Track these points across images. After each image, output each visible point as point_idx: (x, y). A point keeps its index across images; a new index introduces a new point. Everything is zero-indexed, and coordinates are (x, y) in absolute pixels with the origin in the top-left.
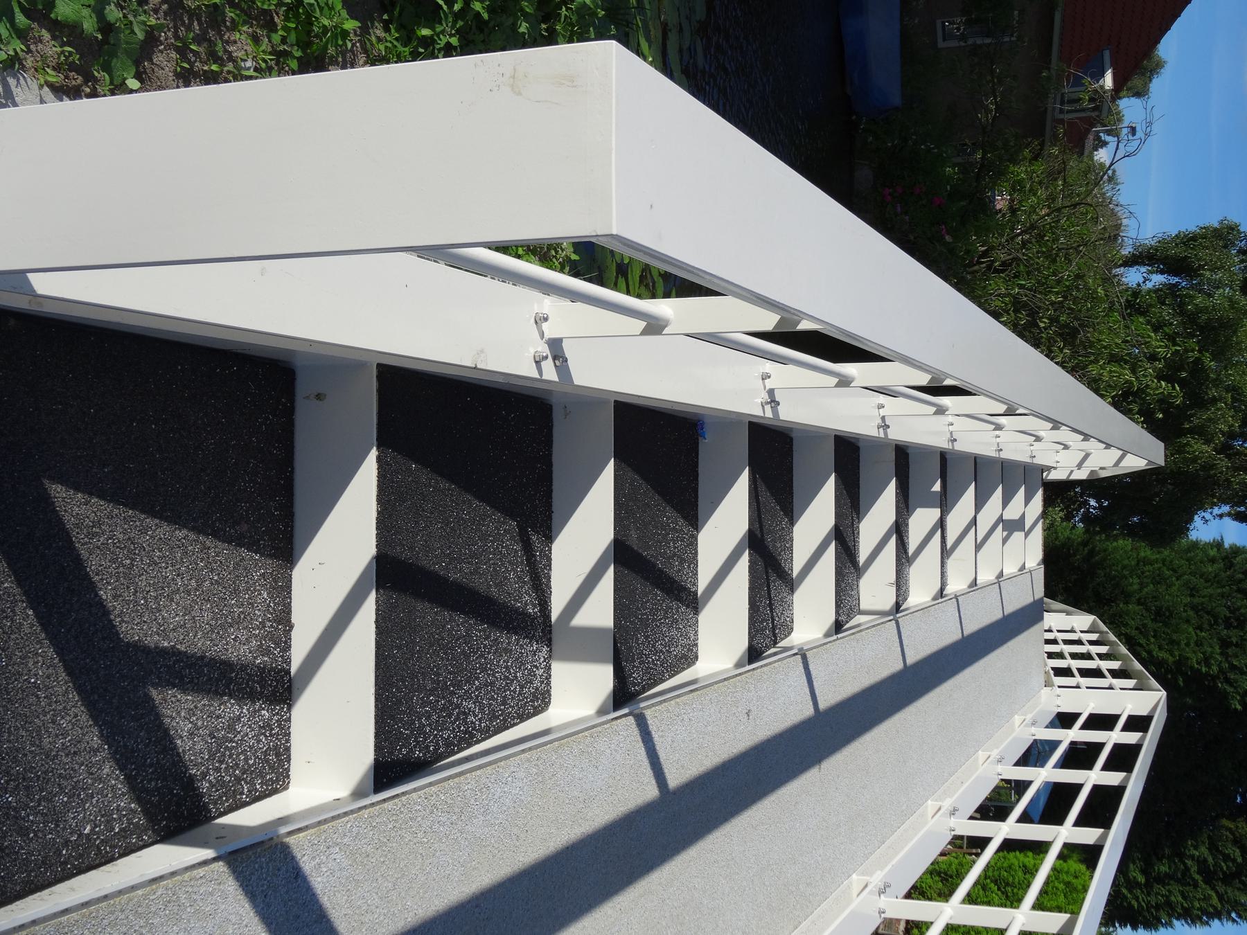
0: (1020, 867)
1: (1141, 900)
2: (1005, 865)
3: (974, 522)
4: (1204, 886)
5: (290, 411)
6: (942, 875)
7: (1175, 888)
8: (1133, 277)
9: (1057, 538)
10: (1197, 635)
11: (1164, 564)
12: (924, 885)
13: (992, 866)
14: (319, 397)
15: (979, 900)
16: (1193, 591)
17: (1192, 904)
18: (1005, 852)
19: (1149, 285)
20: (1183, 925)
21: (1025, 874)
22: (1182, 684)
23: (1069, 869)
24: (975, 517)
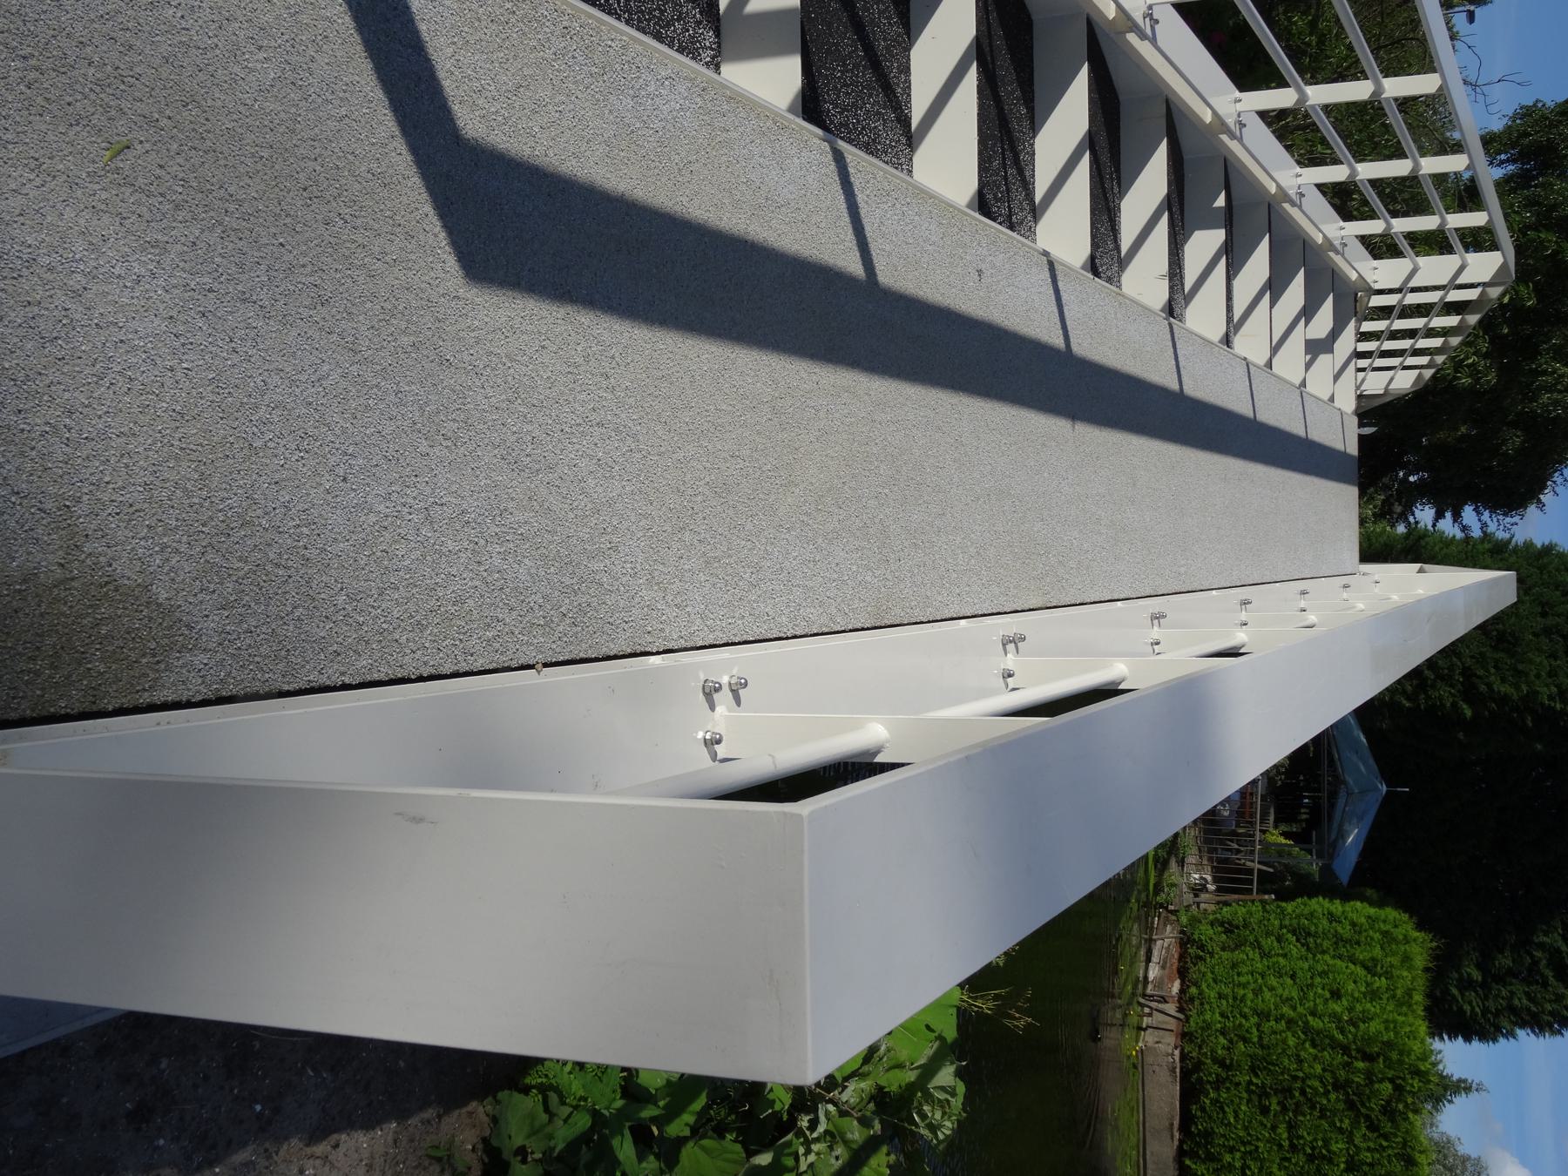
0: (1324, 915)
1: (1474, 1004)
2: (1306, 912)
4: (1555, 983)
6: (1226, 925)
7: (1519, 988)
10: (1550, 665)
12: (1203, 938)
13: (1289, 914)
15: (1273, 953)
17: (1542, 1007)
18: (1306, 898)
20: (1528, 1034)
21: (1331, 923)
22: (1530, 724)
23: (1387, 917)
24: (1271, 359)
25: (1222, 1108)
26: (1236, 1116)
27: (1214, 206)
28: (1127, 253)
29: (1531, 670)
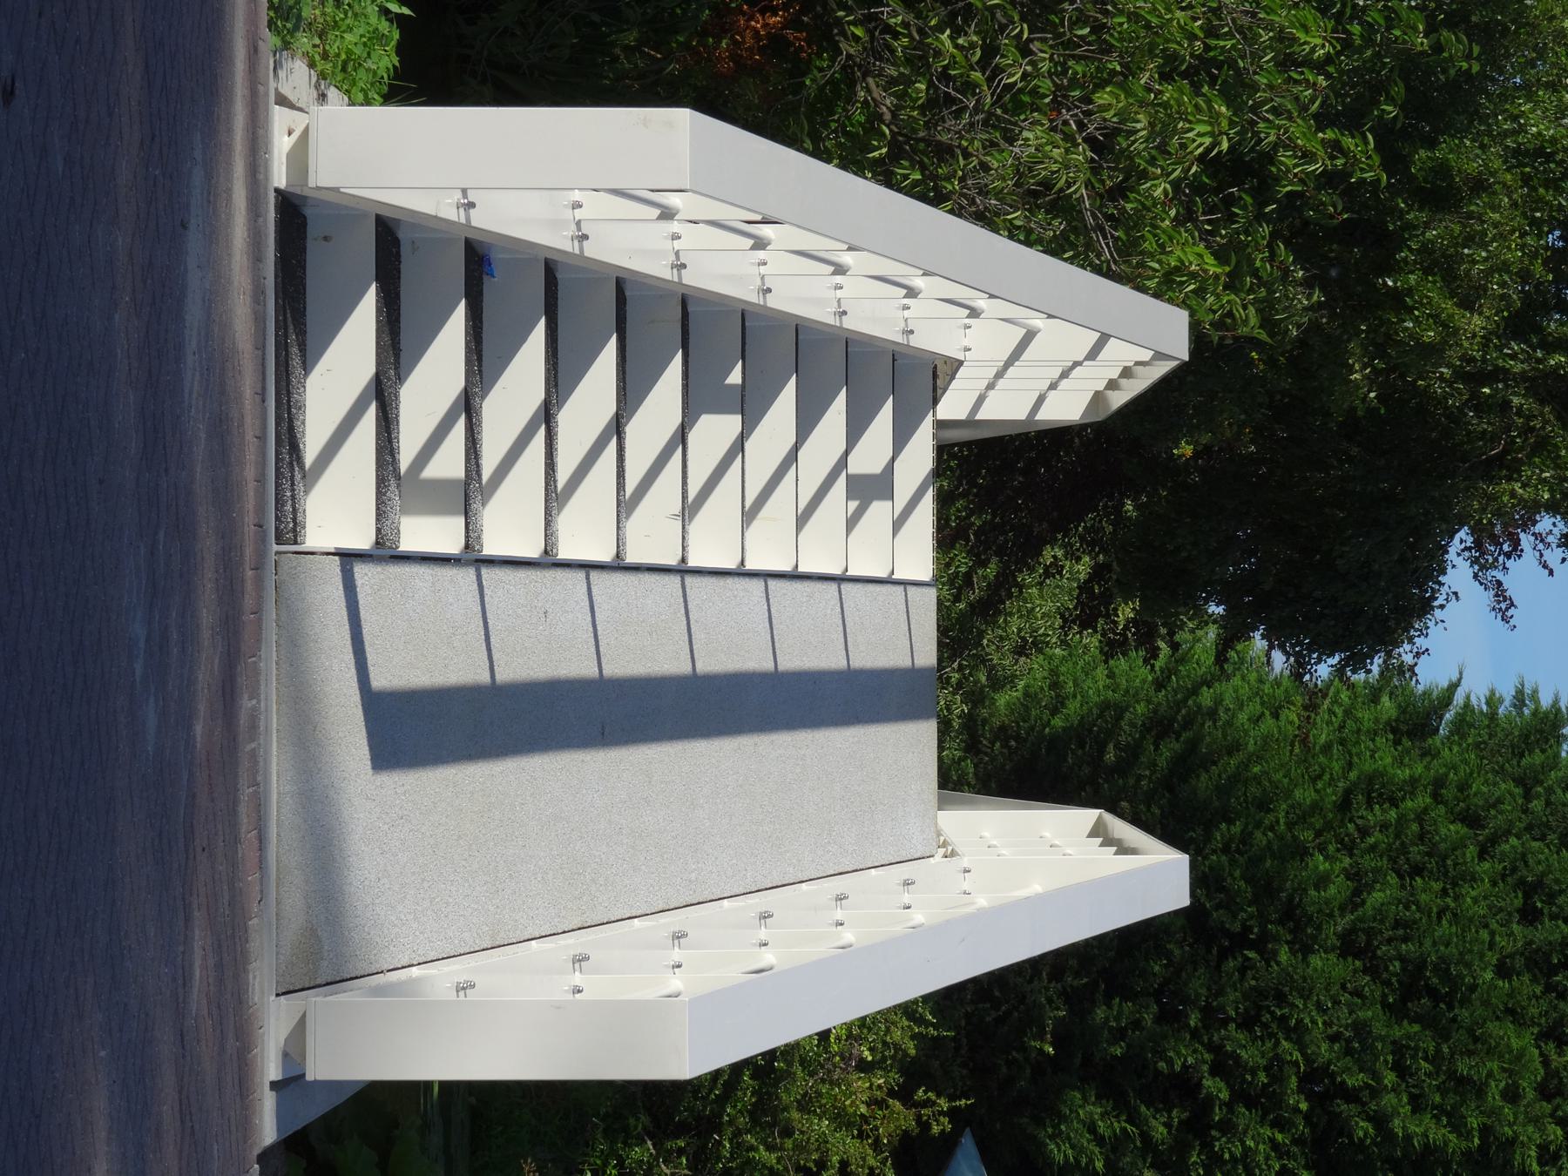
3: (792, 457)
10: (1546, 1062)
11: (1436, 797)
14: (326, 239)
27: (727, 382)
28: (633, 495)
29: (1490, 1074)
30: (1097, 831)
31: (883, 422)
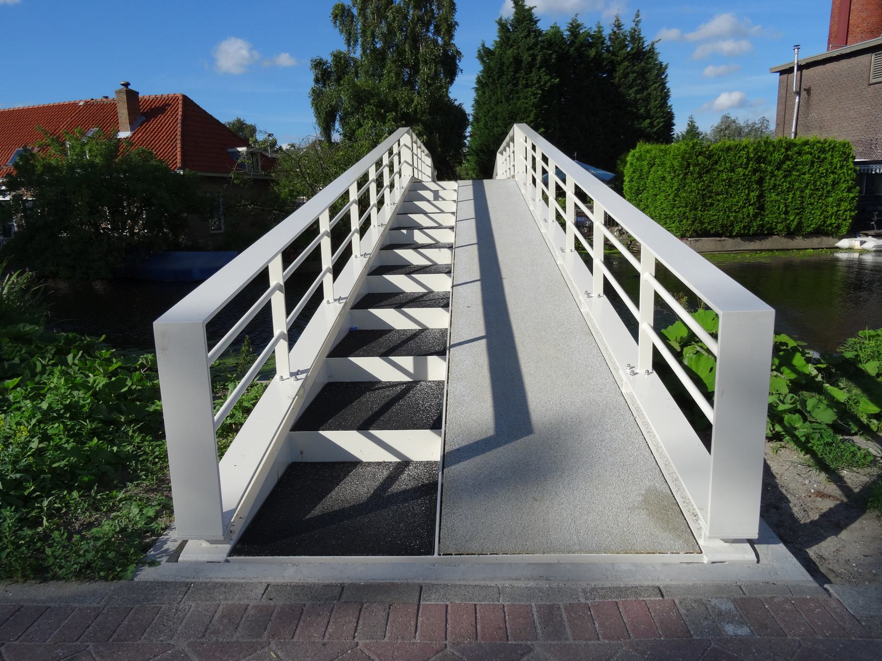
2: (629, 191)
5: (306, 463)
8: (336, 137)
9: (475, 169)
11: (486, 116)
14: (302, 453)
16: (498, 102)
19: (340, 130)
25: (712, 221)
26: (715, 215)
30: (502, 153)
31: (423, 193)
